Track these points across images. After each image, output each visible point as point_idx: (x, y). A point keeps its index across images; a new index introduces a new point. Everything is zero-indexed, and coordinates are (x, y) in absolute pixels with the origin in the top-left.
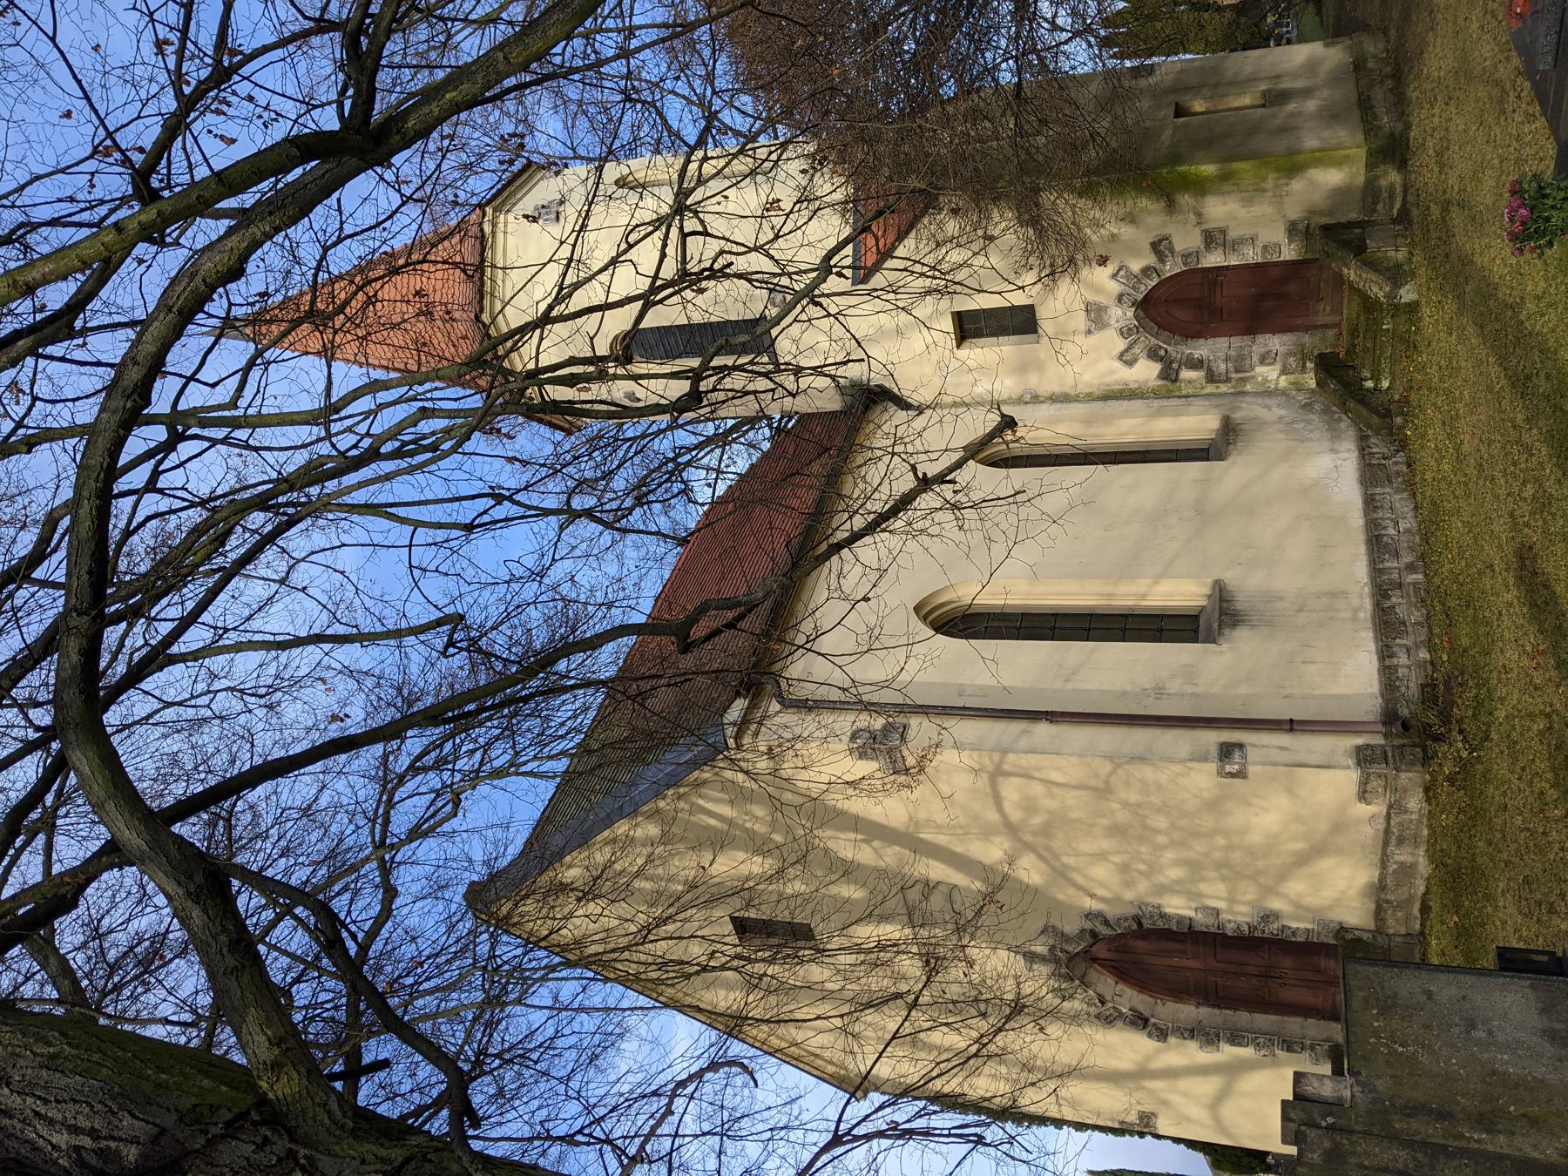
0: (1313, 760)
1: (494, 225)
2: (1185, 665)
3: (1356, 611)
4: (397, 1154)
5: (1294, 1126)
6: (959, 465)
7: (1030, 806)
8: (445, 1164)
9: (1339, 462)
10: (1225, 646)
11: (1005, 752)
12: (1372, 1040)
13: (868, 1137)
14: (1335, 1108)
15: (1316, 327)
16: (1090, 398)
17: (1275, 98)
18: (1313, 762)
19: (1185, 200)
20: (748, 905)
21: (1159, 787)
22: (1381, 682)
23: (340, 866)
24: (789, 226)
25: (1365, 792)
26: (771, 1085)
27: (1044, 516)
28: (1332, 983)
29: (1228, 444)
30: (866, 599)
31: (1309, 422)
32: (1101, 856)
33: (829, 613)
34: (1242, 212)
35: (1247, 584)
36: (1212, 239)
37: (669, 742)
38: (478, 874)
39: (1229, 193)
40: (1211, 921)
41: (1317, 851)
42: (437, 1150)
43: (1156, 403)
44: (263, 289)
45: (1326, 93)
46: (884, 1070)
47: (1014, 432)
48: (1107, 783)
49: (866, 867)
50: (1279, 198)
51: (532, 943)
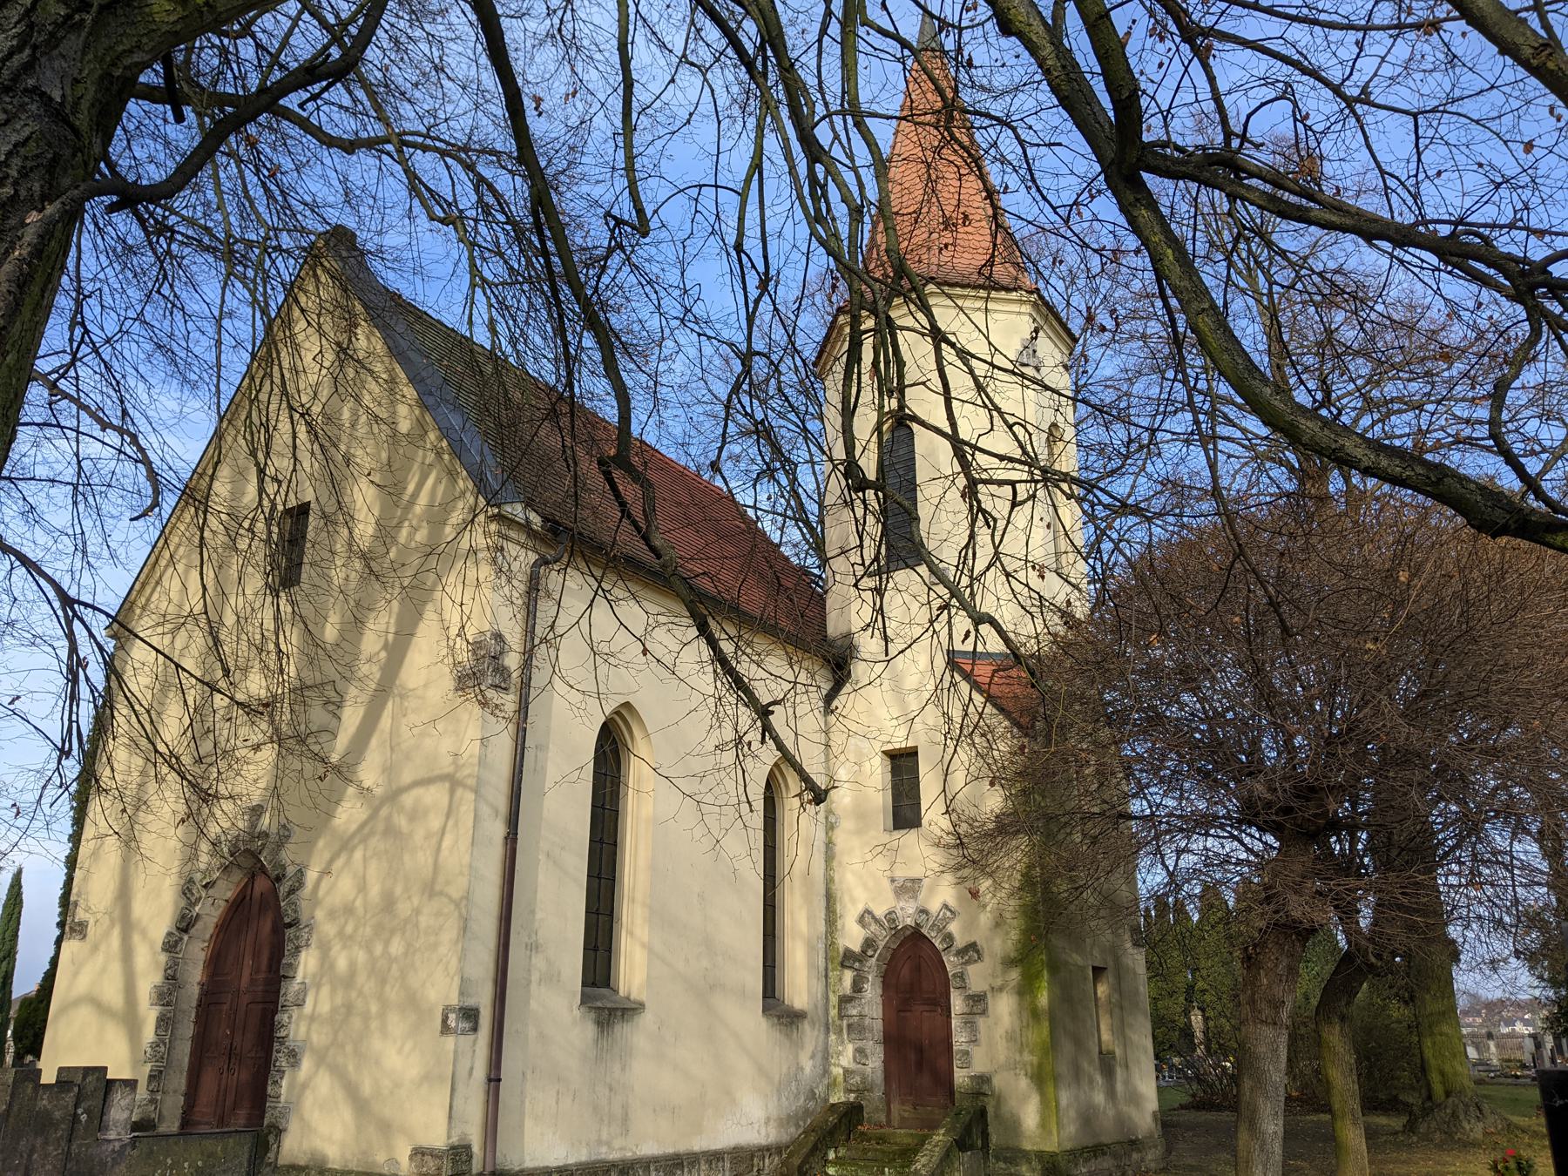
0: (458, 1102)
1: (1021, 302)
2: (559, 973)
3: (608, 1144)
4: (82, 120)
5: (78, 1079)
6: (780, 746)
7: (415, 815)
8: (70, 171)
9: (756, 1126)
10: (577, 1013)
11: (476, 791)
12: (169, 1161)
13: (70, 636)
14: (96, 1122)
15: (888, 1104)
16: (829, 881)
17: (1107, 1064)
18: (455, 1104)
19: (1014, 975)
20: (324, 516)
21: (434, 947)
22: (536, 1169)
23: (380, 98)
24: (1018, 587)
25: (423, 1154)
26: (133, 535)
27: (724, 831)
28: (222, 1122)
29: (779, 1017)
30: (645, 652)
31: (797, 1096)
32: (362, 888)
33: (634, 613)
34: (1000, 1032)
35: (638, 1035)
36: (978, 1002)
37: (500, 447)
38: (366, 238)
39: (1020, 1018)
40: (291, 997)
41: (360, 1106)
42: (86, 164)
43: (821, 946)
44: (975, 63)
45: (1111, 1113)
46: (139, 652)
47: (810, 802)
48: (441, 893)
49: (359, 641)
50: (1012, 1066)
51: (291, 290)
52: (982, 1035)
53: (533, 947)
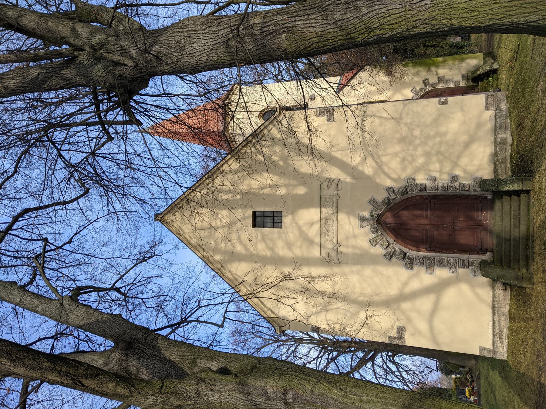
19: (433, 69)
34: (450, 73)
36: (441, 79)
50: (459, 69)
52: (450, 77)
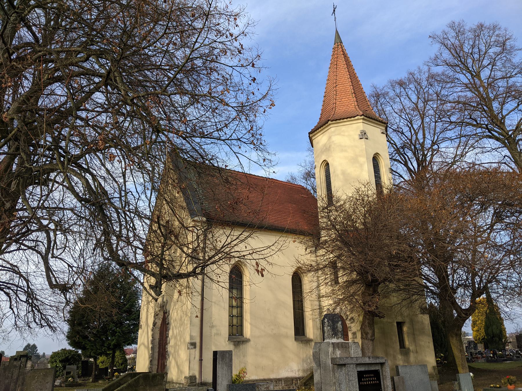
1: (358, 119)
9: (294, 372)
18: (190, 366)
32: (177, 315)
53: (212, 327)
